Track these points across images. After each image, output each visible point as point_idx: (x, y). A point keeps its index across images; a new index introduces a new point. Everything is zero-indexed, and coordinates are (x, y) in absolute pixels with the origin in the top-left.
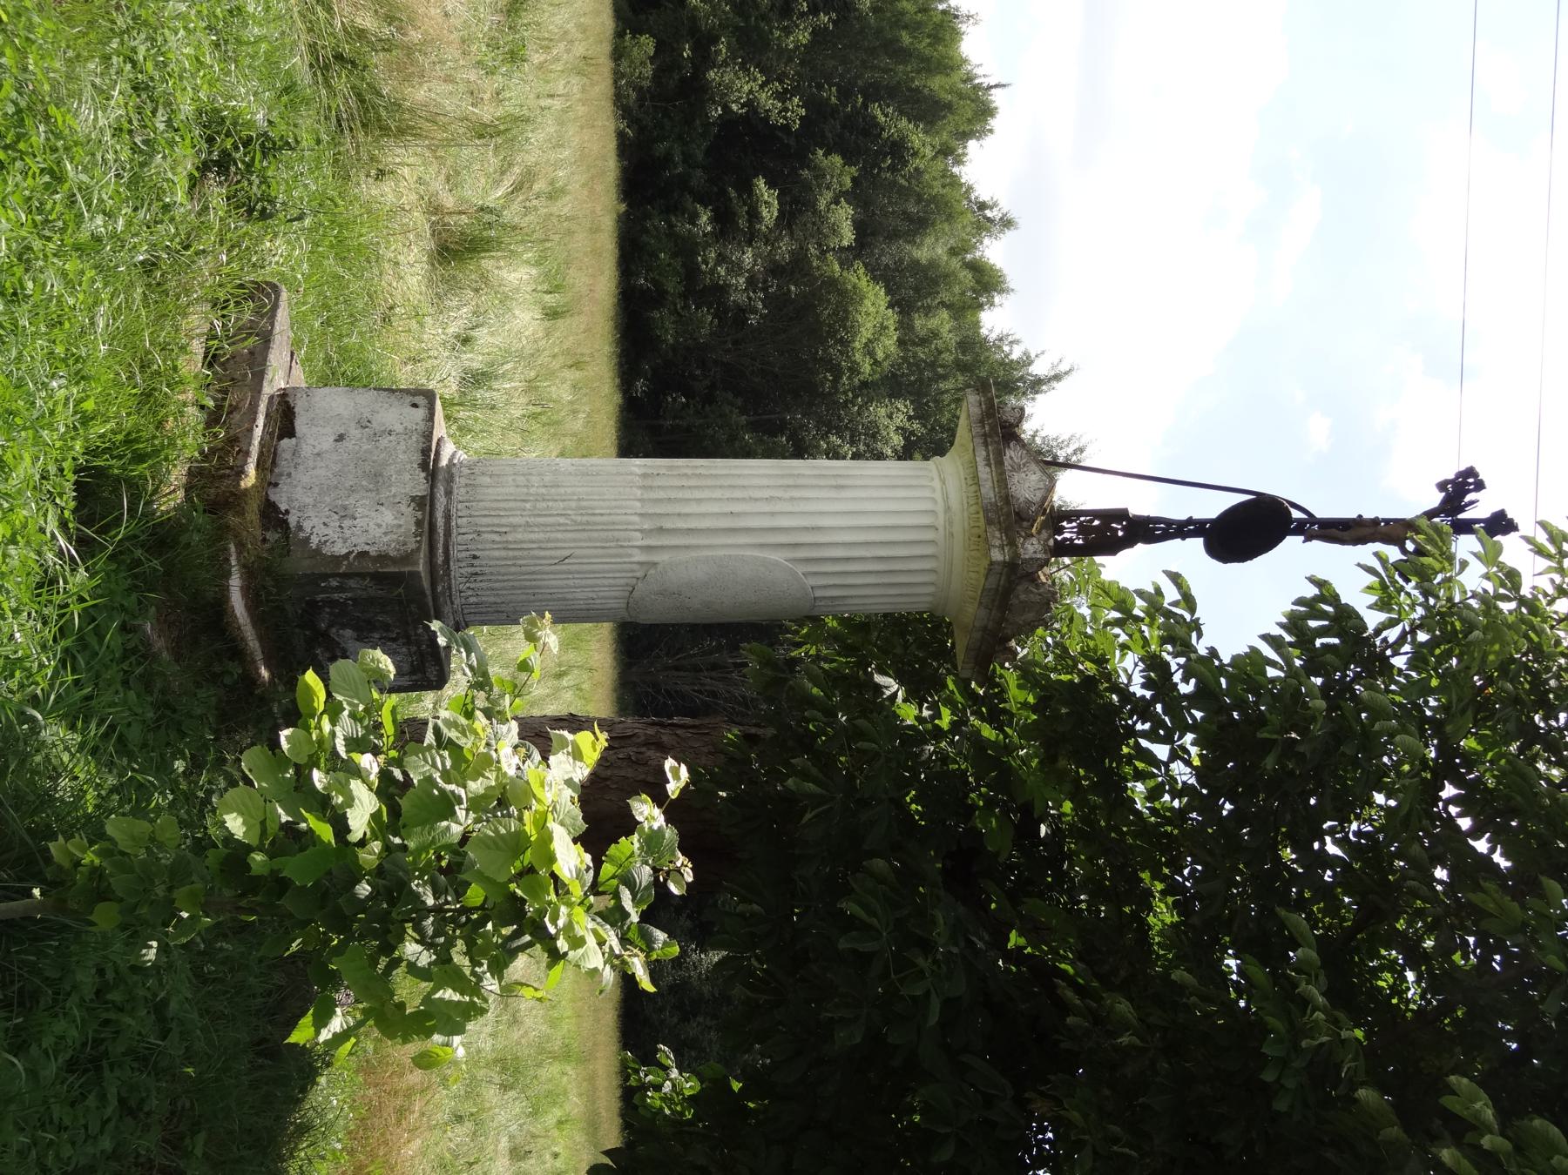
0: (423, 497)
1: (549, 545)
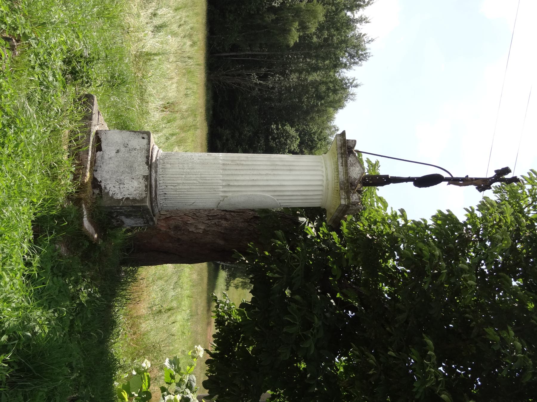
0: (147, 176)
1: (191, 190)
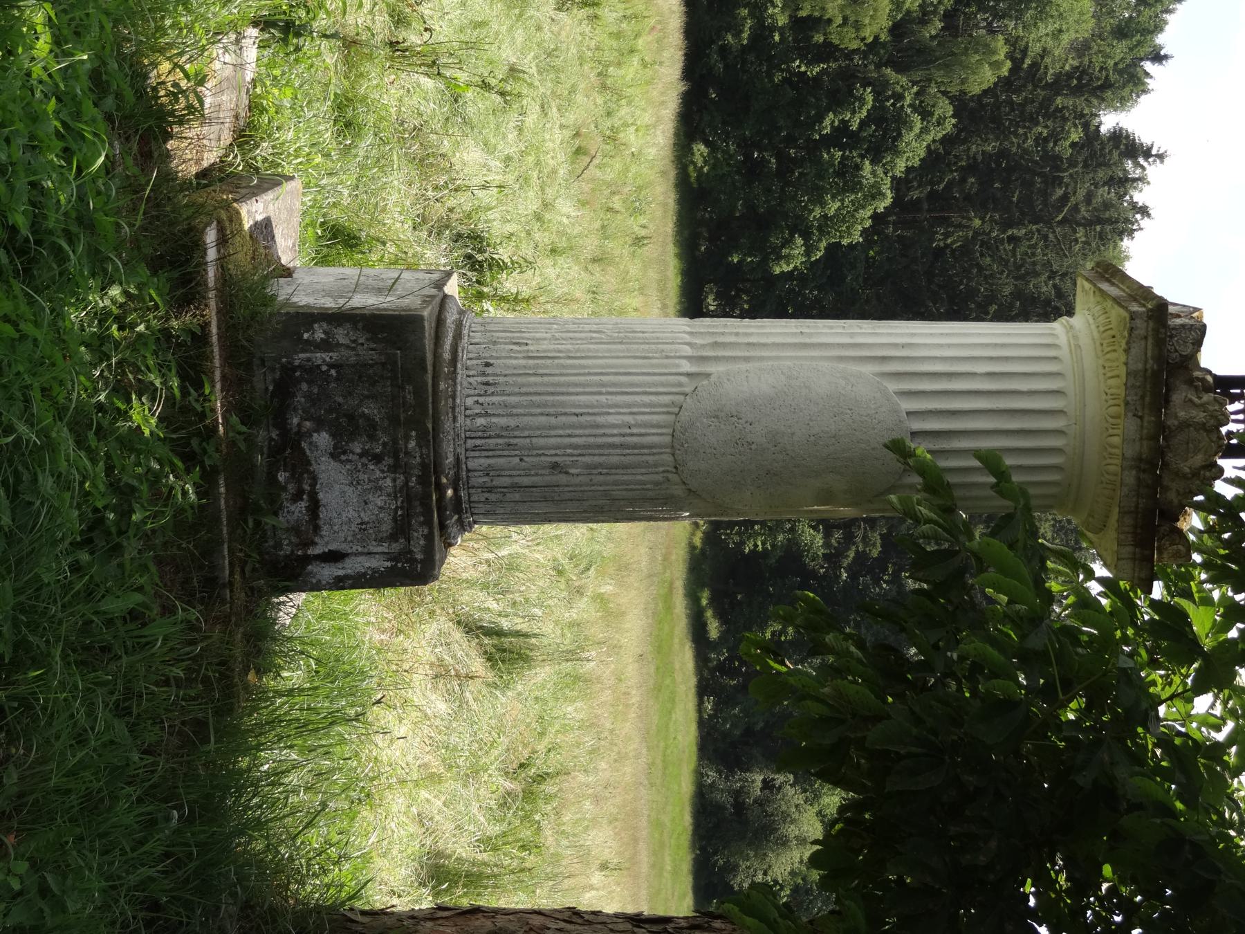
1: (578, 355)
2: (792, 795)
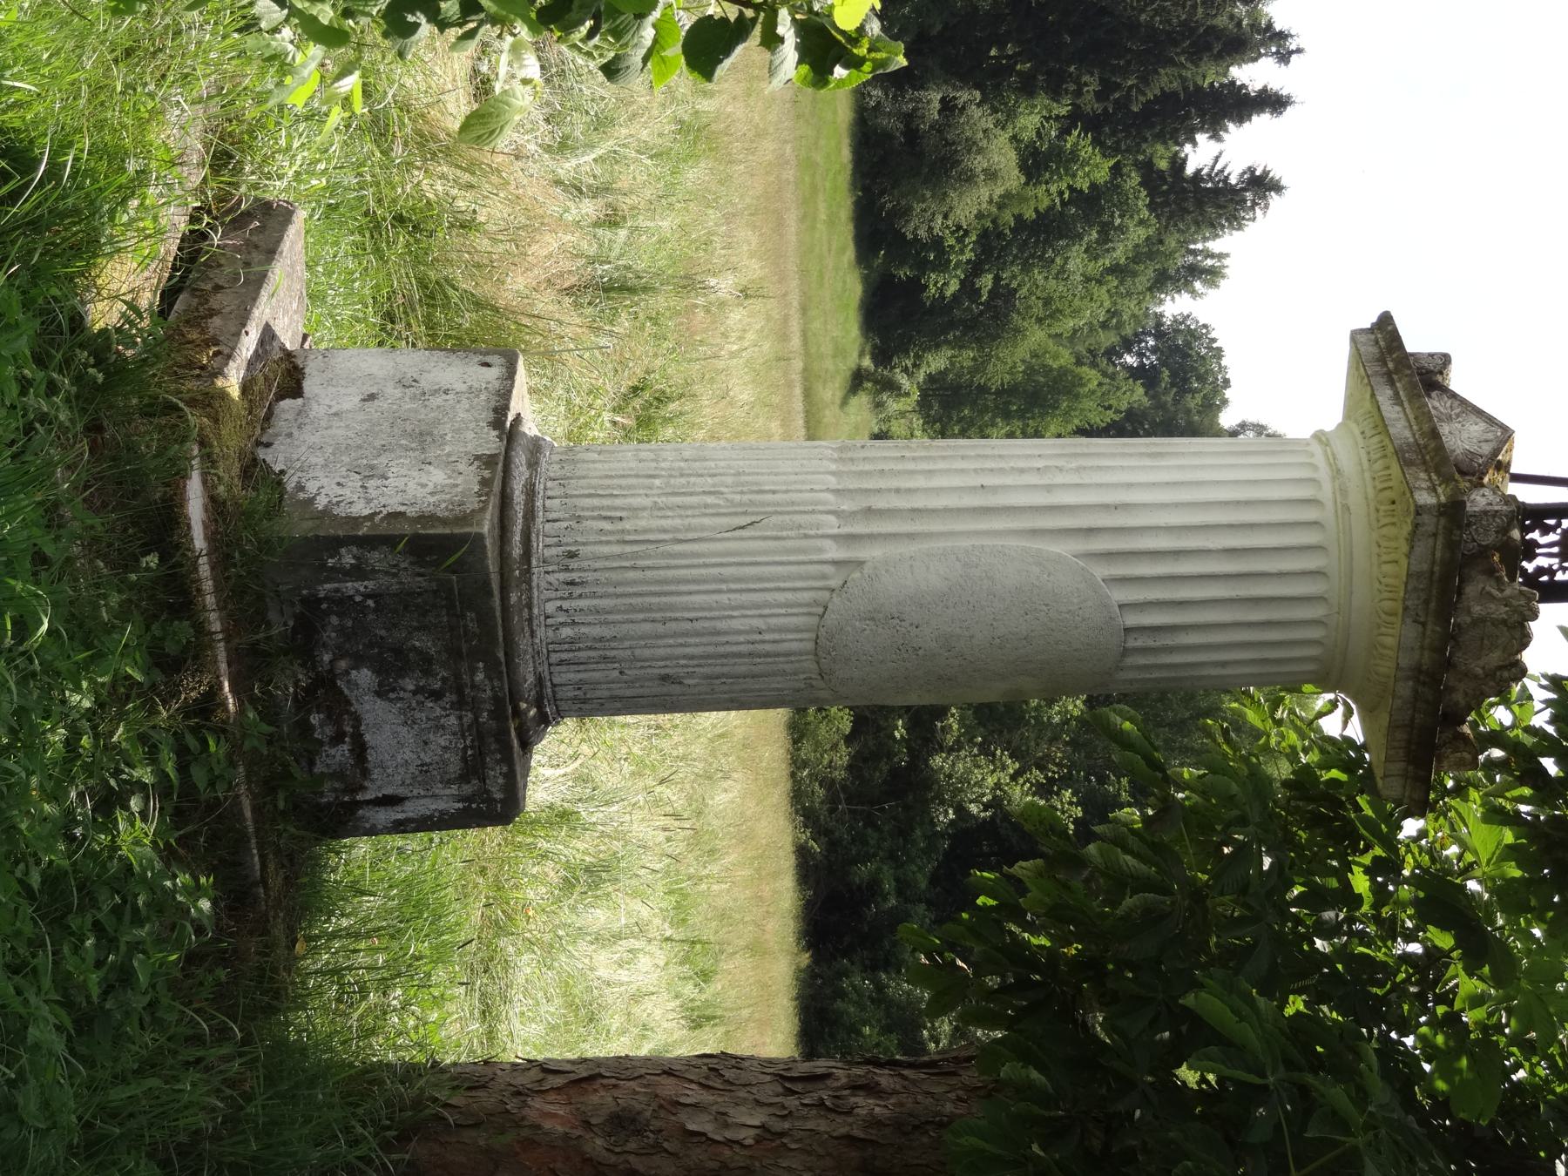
1: (690, 536)
2: (979, 118)
